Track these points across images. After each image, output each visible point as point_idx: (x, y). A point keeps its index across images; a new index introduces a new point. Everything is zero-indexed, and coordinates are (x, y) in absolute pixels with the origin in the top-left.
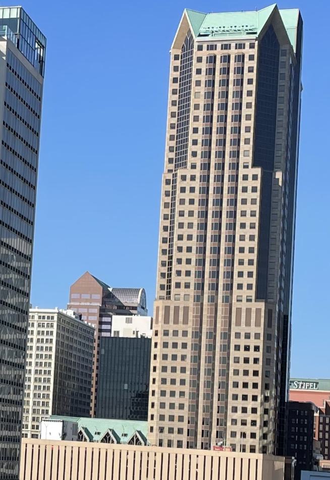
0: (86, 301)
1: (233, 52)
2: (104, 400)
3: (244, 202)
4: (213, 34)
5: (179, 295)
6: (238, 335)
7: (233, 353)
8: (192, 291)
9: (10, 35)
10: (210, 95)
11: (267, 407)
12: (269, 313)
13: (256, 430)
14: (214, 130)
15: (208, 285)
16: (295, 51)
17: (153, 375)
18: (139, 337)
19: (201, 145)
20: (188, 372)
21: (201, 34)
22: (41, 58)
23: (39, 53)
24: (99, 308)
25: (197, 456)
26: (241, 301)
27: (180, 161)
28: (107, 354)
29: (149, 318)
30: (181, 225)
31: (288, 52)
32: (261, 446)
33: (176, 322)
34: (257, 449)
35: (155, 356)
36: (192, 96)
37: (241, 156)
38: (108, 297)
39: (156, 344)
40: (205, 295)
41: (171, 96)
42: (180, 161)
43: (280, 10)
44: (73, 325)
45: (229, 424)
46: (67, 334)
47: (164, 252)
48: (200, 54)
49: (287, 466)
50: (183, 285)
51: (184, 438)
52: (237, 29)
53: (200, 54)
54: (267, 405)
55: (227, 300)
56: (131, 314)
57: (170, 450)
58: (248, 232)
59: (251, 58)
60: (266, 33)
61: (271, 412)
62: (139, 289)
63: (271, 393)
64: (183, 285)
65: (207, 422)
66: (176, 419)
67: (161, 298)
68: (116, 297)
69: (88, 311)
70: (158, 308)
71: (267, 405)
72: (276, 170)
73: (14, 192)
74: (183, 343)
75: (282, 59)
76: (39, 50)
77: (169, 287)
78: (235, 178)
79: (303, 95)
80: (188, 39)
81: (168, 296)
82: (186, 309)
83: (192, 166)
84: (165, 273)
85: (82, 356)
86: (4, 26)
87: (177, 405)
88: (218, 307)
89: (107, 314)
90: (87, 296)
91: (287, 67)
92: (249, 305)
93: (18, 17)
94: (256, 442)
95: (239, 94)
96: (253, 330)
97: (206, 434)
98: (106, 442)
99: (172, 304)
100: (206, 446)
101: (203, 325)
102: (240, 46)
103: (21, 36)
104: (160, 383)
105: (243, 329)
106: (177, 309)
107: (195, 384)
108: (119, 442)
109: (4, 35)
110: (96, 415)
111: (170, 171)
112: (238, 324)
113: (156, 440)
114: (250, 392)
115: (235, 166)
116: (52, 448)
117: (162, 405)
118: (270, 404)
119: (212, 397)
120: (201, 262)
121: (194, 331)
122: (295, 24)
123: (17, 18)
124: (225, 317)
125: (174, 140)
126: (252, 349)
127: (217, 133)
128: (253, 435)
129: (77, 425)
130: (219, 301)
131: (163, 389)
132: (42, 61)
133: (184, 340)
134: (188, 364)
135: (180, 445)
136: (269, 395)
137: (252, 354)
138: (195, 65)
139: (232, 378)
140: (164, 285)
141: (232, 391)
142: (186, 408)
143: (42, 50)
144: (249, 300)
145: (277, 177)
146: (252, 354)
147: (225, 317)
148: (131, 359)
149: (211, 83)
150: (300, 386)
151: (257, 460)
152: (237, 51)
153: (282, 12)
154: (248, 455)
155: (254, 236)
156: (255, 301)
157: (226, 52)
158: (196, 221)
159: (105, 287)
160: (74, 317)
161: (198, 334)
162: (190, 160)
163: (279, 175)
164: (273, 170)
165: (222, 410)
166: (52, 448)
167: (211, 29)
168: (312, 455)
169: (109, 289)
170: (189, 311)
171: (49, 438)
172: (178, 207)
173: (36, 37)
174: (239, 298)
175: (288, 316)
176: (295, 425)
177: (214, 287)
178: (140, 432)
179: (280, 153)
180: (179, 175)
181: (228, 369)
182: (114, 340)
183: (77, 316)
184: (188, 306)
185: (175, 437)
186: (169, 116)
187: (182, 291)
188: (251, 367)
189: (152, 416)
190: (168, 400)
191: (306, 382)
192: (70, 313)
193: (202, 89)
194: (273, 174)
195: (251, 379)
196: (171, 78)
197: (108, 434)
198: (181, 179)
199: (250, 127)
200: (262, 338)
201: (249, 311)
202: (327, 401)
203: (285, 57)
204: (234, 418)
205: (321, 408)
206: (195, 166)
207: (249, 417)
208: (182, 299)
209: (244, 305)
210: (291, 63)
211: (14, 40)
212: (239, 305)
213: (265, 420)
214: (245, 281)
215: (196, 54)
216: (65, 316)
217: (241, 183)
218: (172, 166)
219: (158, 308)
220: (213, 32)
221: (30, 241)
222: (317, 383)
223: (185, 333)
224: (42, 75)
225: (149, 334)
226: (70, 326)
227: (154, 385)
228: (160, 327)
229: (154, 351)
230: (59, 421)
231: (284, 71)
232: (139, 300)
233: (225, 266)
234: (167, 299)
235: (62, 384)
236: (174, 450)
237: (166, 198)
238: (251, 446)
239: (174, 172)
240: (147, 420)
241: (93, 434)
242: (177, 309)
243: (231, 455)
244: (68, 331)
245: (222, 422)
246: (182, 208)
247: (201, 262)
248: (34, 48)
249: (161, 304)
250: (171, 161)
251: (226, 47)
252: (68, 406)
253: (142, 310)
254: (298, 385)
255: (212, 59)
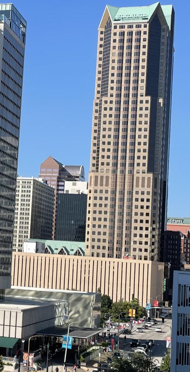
0: (50, 173)
1: (134, 30)
2: (60, 230)
3: (141, 116)
4: (123, 19)
5: (103, 169)
6: (137, 193)
7: (135, 203)
8: (110, 167)
9: (6, 20)
10: (121, 55)
11: (154, 234)
12: (155, 180)
13: (148, 247)
14: (124, 74)
15: (120, 164)
16: (170, 29)
17: (88, 216)
18: (80, 193)
19: (116, 83)
20: (108, 214)
21: (116, 19)
22: (24, 33)
23: (22, 30)
24: (57, 177)
25: (114, 262)
26: (139, 173)
27: (104, 92)
28: (61, 204)
29: (86, 183)
30: (104, 129)
31: (166, 29)
32: (150, 256)
33: (101, 185)
34: (148, 258)
35: (90, 205)
36: (111, 55)
37: (139, 89)
38: (62, 170)
39: (90, 198)
40: (118, 170)
41: (98, 55)
42: (104, 92)
43: (161, 6)
44: (42, 187)
45: (132, 243)
46: (38, 192)
47: (95, 145)
48: (115, 31)
49: (166, 268)
50: (105, 164)
51: (106, 252)
52: (136, 16)
53: (115, 31)
54: (154, 233)
55: (131, 172)
56: (76, 181)
57: (98, 259)
58: (143, 133)
59: (145, 33)
60: (153, 19)
61: (156, 237)
62: (81, 166)
63: (156, 226)
64: (105, 164)
65: (119, 242)
66: (102, 241)
67: (93, 171)
68: (67, 171)
69: (51, 178)
70: (91, 177)
71: (154, 233)
72: (159, 97)
73: (8, 110)
74: (105, 197)
75: (163, 34)
76: (22, 28)
77: (98, 165)
78: (135, 102)
79: (175, 54)
80: (109, 22)
81: (97, 170)
82: (107, 178)
83: (110, 95)
84: (95, 157)
85: (47, 204)
86: (2, 15)
87: (102, 233)
88: (126, 177)
89: (62, 180)
90: (50, 170)
91: (166, 38)
92: (144, 175)
93: (11, 9)
94: (148, 254)
95: (138, 54)
96: (146, 189)
97: (119, 249)
98: (61, 254)
99: (99, 174)
100: (119, 256)
101: (117, 187)
102: (139, 26)
103: (12, 21)
104: (92, 220)
105: (140, 189)
106: (102, 177)
107: (113, 221)
108: (68, 254)
109: (2, 20)
110: (56, 239)
111: (98, 98)
112: (137, 186)
113: (90, 253)
114: (144, 225)
115: (136, 95)
116: (30, 257)
117: (94, 233)
118: (156, 232)
119: (122, 228)
120: (116, 151)
121: (112, 190)
122: (170, 13)
123: (10, 10)
124: (129, 182)
125: (100, 80)
126: (145, 200)
127: (125, 77)
128: (146, 250)
129: (44, 244)
130: (126, 173)
131: (94, 224)
132: (24, 35)
133: (106, 195)
134: (108, 209)
135: (104, 255)
136: (155, 227)
137: (145, 204)
138: (113, 37)
139: (134, 217)
140: (95, 164)
141: (134, 225)
142: (107, 234)
143: (24, 28)
144: (143, 173)
145: (160, 102)
146: (145, 204)
147: (130, 182)
148: (76, 206)
149: (122, 48)
150: (173, 222)
151: (148, 265)
152: (137, 29)
153: (162, 7)
154: (143, 261)
155: (146, 135)
156: (147, 173)
157: (130, 29)
158: (113, 127)
159: (61, 165)
160: (43, 182)
161: (114, 192)
162: (110, 92)
163: (161, 100)
164: (157, 98)
165: (128, 235)
166: (30, 257)
167: (122, 16)
168: (180, 261)
169: (63, 166)
170: (109, 178)
171: (28, 251)
172: (103, 119)
173: (21, 21)
174: (138, 171)
175: (166, 182)
176: (170, 244)
177: (124, 165)
178: (80, 248)
179: (162, 87)
180: (103, 100)
181: (132, 212)
182: (66, 195)
183: (44, 181)
184: (108, 176)
185: (101, 251)
186: (97, 67)
187: (105, 167)
188: (145, 211)
189: (88, 239)
190: (97, 230)
191: (176, 220)
192: (40, 180)
193: (117, 51)
194: (158, 100)
195: (145, 218)
196: (99, 45)
197: (62, 249)
198: (105, 102)
199: (144, 73)
200: (151, 194)
201: (143, 178)
202: (189, 230)
203: (164, 33)
204: (135, 240)
205: (185, 234)
206: (113, 95)
207: (144, 240)
208: (105, 172)
209: (141, 175)
210: (168, 36)
211: (8, 23)
212: (138, 175)
213: (153, 241)
214: (141, 161)
215: (113, 31)
216: (38, 182)
217: (139, 105)
218: (99, 95)
219: (91, 177)
220: (123, 18)
221: (17, 138)
222: (183, 220)
223: (107, 192)
224: (24, 43)
225: (86, 192)
226: (40, 187)
227: (89, 221)
228: (92, 188)
229: (89, 202)
230: (34, 242)
231: (164, 40)
232: (80, 172)
233: (130, 152)
234: (96, 172)
235: (36, 221)
236: (100, 259)
237: (96, 113)
238: (144, 256)
239: (100, 99)
240: (85, 242)
241: (54, 250)
242: (102, 177)
243: (133, 261)
244: (39, 190)
245: (128, 243)
246: (105, 119)
247: (116, 151)
248: (19, 27)
249: (93, 175)
250: (98, 92)
251: (130, 27)
252: (39, 234)
253: (82, 178)
254: (172, 221)
255: (122, 34)
